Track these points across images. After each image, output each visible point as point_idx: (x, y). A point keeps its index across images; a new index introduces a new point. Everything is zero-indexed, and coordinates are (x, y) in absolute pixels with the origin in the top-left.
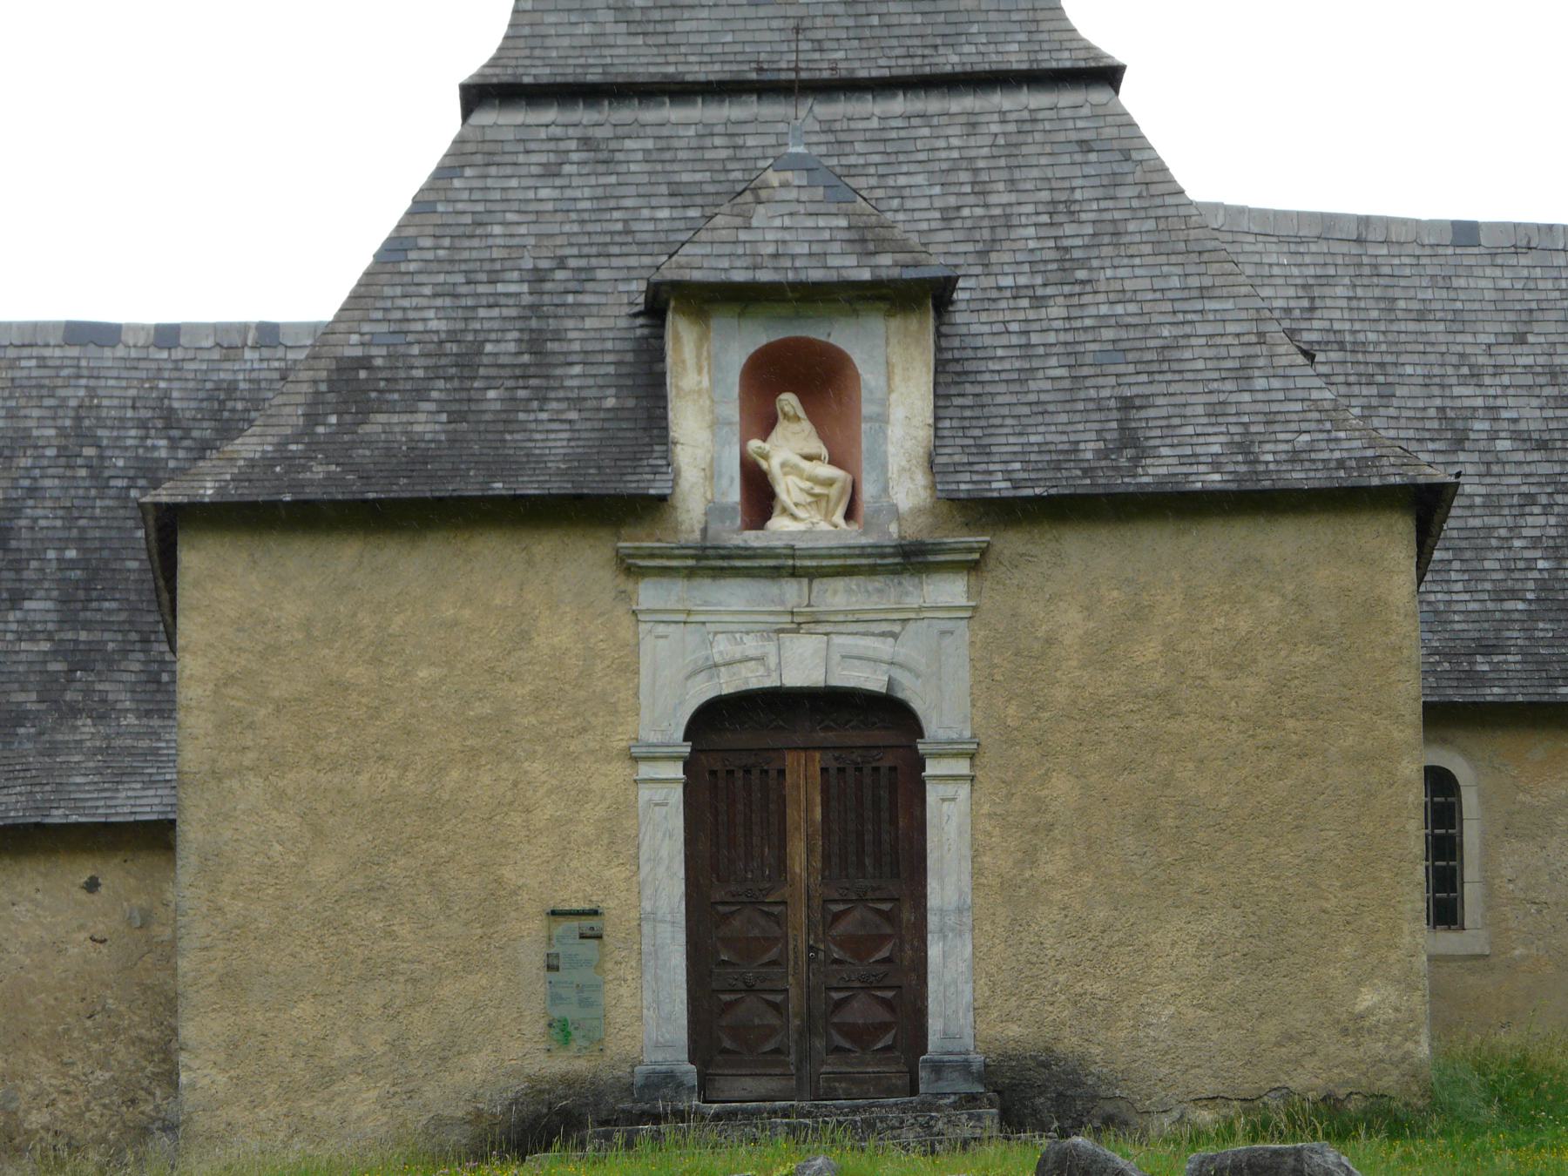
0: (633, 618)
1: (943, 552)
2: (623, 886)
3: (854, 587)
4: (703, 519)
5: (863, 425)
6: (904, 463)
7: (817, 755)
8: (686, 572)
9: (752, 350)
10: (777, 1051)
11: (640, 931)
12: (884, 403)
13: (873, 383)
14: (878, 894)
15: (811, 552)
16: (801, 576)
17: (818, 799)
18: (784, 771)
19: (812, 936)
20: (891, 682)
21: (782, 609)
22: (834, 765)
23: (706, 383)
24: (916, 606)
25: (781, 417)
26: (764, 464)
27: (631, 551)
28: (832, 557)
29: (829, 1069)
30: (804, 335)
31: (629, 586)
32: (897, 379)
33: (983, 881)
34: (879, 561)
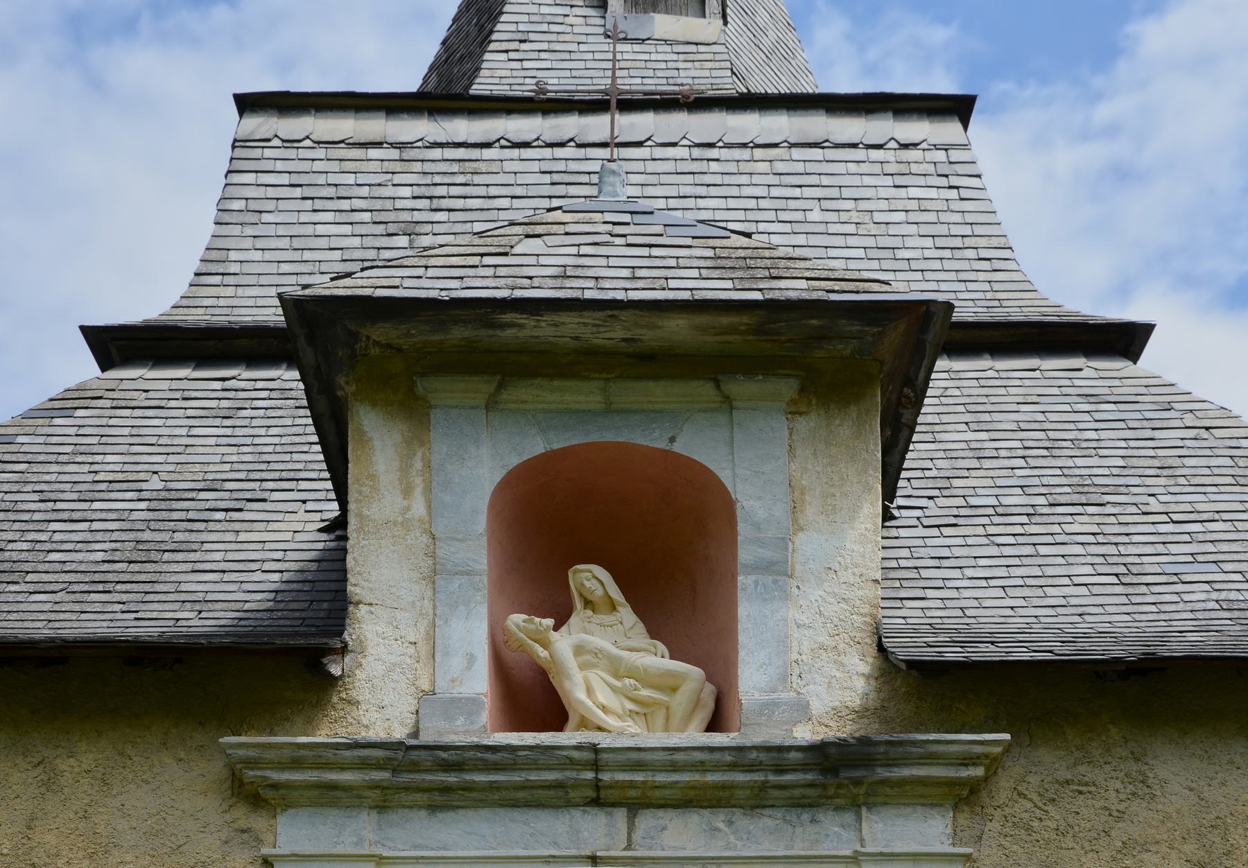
1: (907, 761)
3: (721, 825)
4: (411, 720)
5: (740, 578)
6: (823, 639)
8: (375, 795)
9: (514, 461)
12: (783, 543)
13: (761, 514)
15: (634, 756)
16: (614, 805)
21: (573, 852)
23: (419, 508)
24: (848, 853)
25: (578, 604)
26: (542, 653)
27: (251, 753)
28: (674, 767)
30: (623, 437)
31: (259, 822)
32: (810, 512)
34: (772, 778)
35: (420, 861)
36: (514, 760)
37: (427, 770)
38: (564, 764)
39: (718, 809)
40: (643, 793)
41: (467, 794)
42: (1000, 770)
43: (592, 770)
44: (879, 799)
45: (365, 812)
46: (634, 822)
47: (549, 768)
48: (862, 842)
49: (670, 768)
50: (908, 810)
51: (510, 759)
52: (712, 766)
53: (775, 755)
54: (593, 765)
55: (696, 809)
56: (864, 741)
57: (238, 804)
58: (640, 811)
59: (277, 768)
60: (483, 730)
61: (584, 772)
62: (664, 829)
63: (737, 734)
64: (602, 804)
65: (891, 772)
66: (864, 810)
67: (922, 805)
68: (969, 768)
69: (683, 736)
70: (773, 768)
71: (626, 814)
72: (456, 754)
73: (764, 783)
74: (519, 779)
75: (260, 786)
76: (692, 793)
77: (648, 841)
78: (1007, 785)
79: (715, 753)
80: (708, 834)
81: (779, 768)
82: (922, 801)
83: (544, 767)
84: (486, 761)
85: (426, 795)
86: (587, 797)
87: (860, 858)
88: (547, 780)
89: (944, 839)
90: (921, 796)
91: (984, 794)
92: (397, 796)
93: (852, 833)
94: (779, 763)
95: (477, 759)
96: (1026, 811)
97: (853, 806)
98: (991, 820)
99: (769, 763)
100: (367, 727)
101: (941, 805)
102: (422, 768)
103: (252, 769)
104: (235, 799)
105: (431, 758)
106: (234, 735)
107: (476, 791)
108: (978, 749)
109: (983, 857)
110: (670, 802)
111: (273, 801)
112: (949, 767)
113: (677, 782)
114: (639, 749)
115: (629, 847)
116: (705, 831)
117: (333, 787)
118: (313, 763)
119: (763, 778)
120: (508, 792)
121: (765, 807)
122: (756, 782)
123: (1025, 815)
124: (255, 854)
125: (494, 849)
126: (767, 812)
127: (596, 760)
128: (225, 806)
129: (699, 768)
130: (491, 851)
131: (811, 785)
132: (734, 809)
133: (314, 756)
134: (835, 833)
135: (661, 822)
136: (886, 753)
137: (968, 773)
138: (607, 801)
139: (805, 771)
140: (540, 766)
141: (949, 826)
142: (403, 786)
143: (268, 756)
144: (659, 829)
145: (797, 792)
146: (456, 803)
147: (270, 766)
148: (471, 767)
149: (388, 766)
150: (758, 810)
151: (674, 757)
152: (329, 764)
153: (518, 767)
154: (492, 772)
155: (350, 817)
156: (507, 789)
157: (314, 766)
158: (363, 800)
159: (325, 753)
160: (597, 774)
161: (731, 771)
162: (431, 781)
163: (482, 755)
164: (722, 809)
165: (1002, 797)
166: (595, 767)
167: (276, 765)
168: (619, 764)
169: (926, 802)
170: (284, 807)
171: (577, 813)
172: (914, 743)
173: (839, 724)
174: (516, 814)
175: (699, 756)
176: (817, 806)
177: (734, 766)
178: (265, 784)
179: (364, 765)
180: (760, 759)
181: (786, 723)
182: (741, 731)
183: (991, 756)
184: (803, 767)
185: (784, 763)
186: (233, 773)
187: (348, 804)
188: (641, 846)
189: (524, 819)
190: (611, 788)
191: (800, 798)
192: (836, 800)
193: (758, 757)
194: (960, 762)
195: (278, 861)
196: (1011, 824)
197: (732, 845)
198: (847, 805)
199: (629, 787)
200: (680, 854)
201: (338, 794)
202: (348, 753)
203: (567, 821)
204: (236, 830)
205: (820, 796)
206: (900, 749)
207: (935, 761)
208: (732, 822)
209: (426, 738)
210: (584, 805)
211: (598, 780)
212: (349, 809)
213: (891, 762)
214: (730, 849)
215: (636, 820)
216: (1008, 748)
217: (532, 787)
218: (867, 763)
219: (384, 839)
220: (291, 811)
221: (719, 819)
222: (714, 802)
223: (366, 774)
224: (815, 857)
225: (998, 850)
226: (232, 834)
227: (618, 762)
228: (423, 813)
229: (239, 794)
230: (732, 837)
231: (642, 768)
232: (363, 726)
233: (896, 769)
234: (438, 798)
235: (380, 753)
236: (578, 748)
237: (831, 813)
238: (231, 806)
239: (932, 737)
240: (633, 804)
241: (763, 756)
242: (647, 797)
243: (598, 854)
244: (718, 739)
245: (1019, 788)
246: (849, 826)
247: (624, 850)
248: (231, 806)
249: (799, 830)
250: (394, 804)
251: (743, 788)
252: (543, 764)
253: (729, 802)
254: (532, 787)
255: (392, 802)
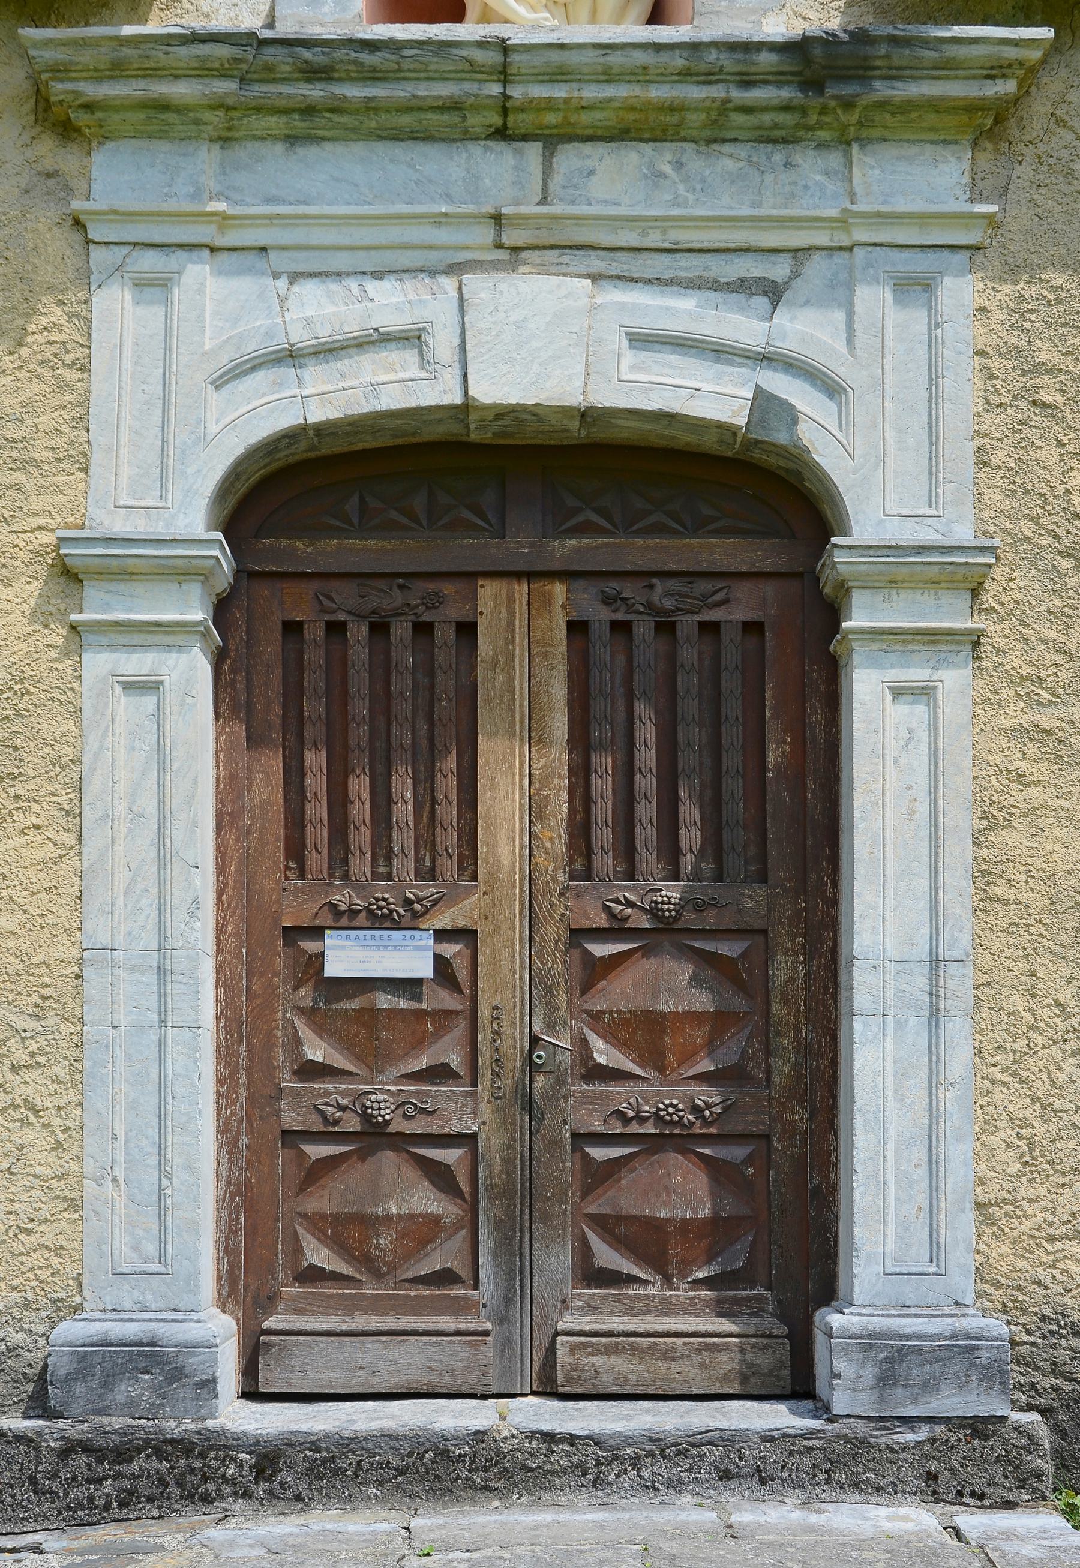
0: (78, 237)
2: (41, 879)
3: (667, 169)
7: (559, 591)
8: (215, 118)
10: (445, 1278)
11: (79, 992)
14: (711, 918)
16: (525, 138)
17: (559, 693)
18: (474, 625)
19: (539, 1011)
20: (762, 401)
21: (470, 208)
22: (601, 615)
24: (834, 213)
27: (60, 55)
28: (608, 76)
29: (586, 1323)
31: (68, 160)
33: (1002, 890)
34: (738, 95)
35: (275, 221)
36: (398, 63)
37: (285, 79)
38: (463, 71)
39: (664, 144)
40: (565, 118)
41: (337, 118)
42: (1033, 89)
43: (499, 81)
44: (875, 133)
45: (205, 148)
46: (551, 163)
47: (443, 78)
48: (852, 197)
49: (602, 78)
50: (914, 150)
51: (392, 61)
52: (657, 75)
53: (740, 56)
54: (500, 73)
55: (634, 143)
56: (860, 37)
57: (43, 136)
58: (560, 146)
59: (91, 78)
60: (357, 20)
61: (488, 85)
62: (592, 173)
63: (689, 27)
64: (510, 136)
65: (893, 88)
66: (855, 148)
67: (932, 142)
68: (997, 81)
69: (618, 31)
70: (738, 78)
71: (541, 151)
72: (323, 53)
73: (726, 101)
74: (402, 94)
75: (70, 107)
76: (631, 117)
77: (570, 191)
78: (1042, 109)
79: (662, 53)
80: (649, 181)
81: (745, 78)
82: (932, 136)
83: (437, 75)
84: (362, 64)
85: (284, 119)
86: (490, 126)
87: (851, 220)
88: (440, 97)
89: (959, 192)
90: (931, 129)
91: (1012, 123)
92: (245, 121)
93: (839, 184)
94: (744, 69)
95: (350, 62)
96: (1065, 147)
97: (841, 143)
98: (1020, 162)
99: (732, 71)
100: (208, 16)
101: (956, 142)
102: (278, 76)
103: (61, 80)
104: (39, 129)
105: (290, 60)
106: (37, 27)
107: (348, 113)
108: (1011, 53)
109: (1008, 219)
110: (600, 132)
111: (87, 130)
112: (971, 82)
113: (610, 100)
114: (562, 46)
115: (544, 201)
116: (646, 177)
117: (163, 106)
118: (139, 69)
119: (723, 94)
120: (388, 116)
121: (724, 141)
122: (714, 100)
123: (1064, 153)
124: (64, 210)
125: (369, 204)
126: (727, 148)
127: (505, 65)
128: (26, 137)
129: (641, 78)
130: (366, 207)
131: (786, 108)
132: (684, 144)
133: (140, 56)
134: (817, 183)
135: (588, 163)
136: (887, 56)
137: (996, 89)
138: (517, 132)
139: (779, 84)
140: (431, 74)
141: (966, 173)
142: (253, 104)
143: (82, 59)
144: (585, 173)
145: (767, 118)
146: (321, 133)
147: (84, 74)
148: (343, 75)
149: (236, 73)
150: (715, 146)
151: (608, 58)
152: (159, 69)
153: (402, 75)
154: (368, 83)
155: (184, 155)
156: (388, 111)
157: (140, 73)
158: (201, 128)
159: (154, 52)
160: (505, 87)
161: (681, 82)
162: (289, 96)
163: (357, 55)
164: (668, 144)
165: (1036, 127)
166: (502, 77)
167: (91, 73)
168: (536, 71)
169: (936, 137)
170: (101, 139)
171: (476, 149)
172: (926, 43)
173: (821, 16)
174: (399, 150)
175: (641, 58)
176: (792, 142)
177: (686, 75)
178: (77, 103)
179: (204, 71)
180: (720, 63)
181: (753, 11)
182: (695, 23)
183: (1027, 64)
184: (777, 78)
185: (753, 69)
186: (38, 90)
187: (183, 135)
188: (561, 200)
189: (408, 159)
190: (523, 110)
191: (771, 128)
192: (818, 133)
193: (718, 59)
194: (985, 72)
195: (92, 220)
196: (1046, 168)
197: (681, 200)
198: (832, 140)
199: (544, 109)
200: (612, 211)
201: (171, 117)
202: (183, 51)
203: (463, 161)
204: (39, 173)
205: (797, 126)
206: (907, 52)
207: (952, 73)
208: (682, 164)
209: (285, 29)
210: (486, 139)
211: (506, 97)
212: (184, 143)
213: (894, 72)
214: (679, 205)
215: (554, 160)
216: (1055, 47)
217: (420, 109)
218: (861, 72)
219: (228, 188)
220: (110, 145)
221: (664, 157)
222: (658, 133)
223: (207, 85)
224: (791, 219)
225: (1028, 208)
226: (35, 179)
227: (534, 67)
228: (279, 148)
229: (45, 120)
230: (681, 187)
231: (564, 77)
232: (203, 14)
233: (899, 84)
234: (298, 123)
235: (223, 51)
236: (482, 44)
237: (812, 152)
238: (33, 138)
239: (957, 31)
240: (550, 135)
241: (726, 61)
242: (570, 124)
243: (504, 211)
244: (662, 33)
245: (1058, 113)
246: (836, 173)
247: (538, 204)
248: (33, 138)
249: (769, 178)
250: (242, 133)
251: (696, 109)
252: (436, 71)
253: (678, 133)
254: (420, 109)
255: (238, 131)
